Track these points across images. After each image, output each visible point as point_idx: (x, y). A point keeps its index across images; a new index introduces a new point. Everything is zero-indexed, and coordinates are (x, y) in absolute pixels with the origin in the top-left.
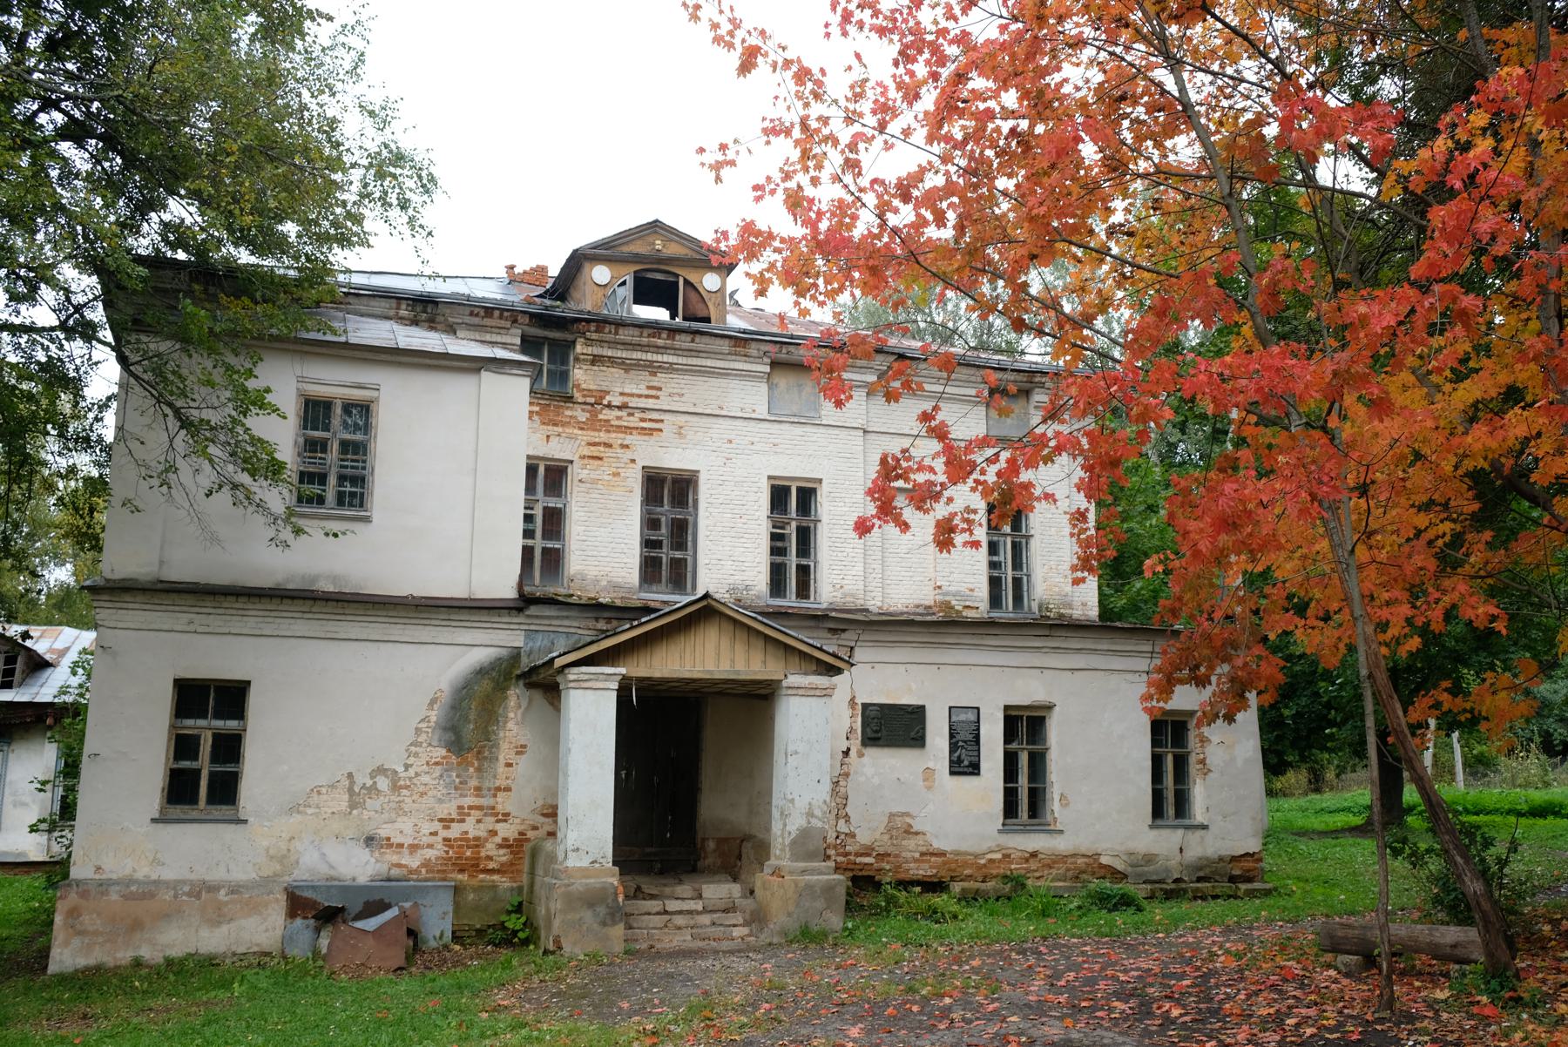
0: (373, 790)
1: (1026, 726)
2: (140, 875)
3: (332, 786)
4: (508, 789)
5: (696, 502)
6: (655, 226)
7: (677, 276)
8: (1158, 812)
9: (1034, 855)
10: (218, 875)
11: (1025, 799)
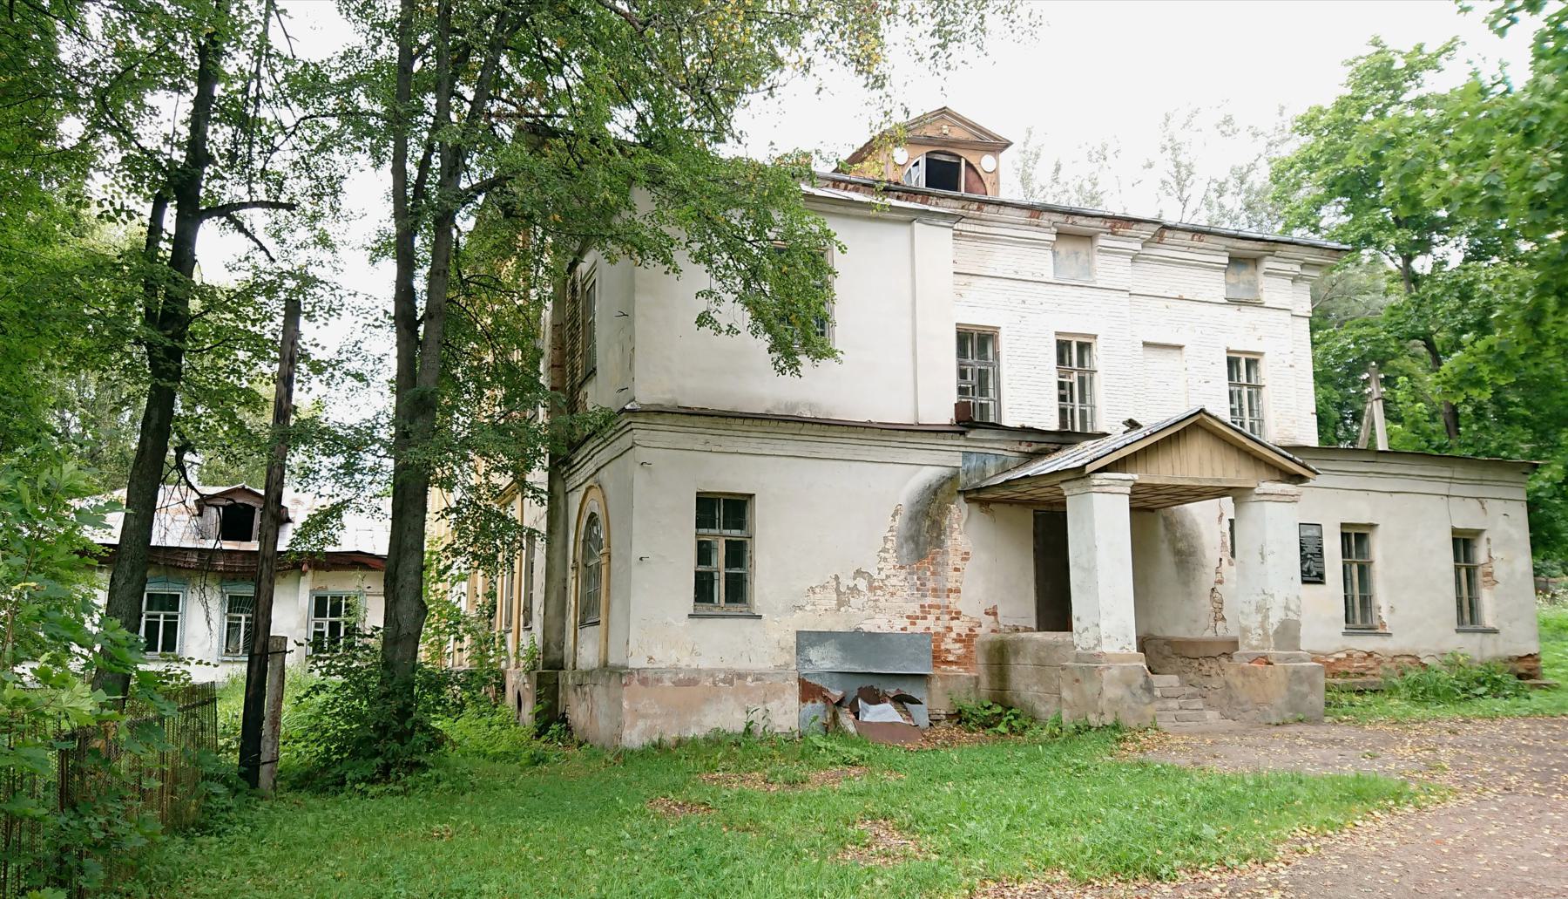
0: (854, 590)
1: (1356, 539)
2: (682, 664)
3: (824, 587)
4: (958, 591)
5: (996, 355)
6: (944, 111)
7: (960, 157)
8: (1460, 621)
9: (1370, 655)
10: (741, 665)
11: (1359, 610)
